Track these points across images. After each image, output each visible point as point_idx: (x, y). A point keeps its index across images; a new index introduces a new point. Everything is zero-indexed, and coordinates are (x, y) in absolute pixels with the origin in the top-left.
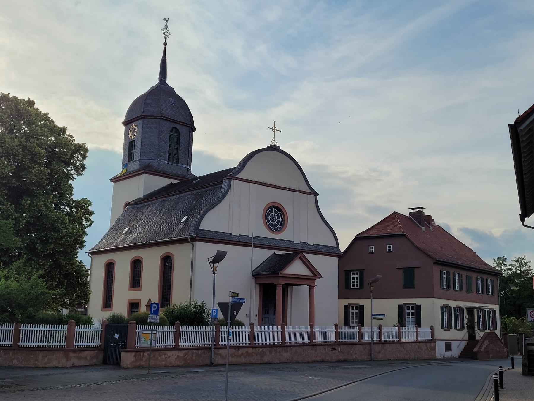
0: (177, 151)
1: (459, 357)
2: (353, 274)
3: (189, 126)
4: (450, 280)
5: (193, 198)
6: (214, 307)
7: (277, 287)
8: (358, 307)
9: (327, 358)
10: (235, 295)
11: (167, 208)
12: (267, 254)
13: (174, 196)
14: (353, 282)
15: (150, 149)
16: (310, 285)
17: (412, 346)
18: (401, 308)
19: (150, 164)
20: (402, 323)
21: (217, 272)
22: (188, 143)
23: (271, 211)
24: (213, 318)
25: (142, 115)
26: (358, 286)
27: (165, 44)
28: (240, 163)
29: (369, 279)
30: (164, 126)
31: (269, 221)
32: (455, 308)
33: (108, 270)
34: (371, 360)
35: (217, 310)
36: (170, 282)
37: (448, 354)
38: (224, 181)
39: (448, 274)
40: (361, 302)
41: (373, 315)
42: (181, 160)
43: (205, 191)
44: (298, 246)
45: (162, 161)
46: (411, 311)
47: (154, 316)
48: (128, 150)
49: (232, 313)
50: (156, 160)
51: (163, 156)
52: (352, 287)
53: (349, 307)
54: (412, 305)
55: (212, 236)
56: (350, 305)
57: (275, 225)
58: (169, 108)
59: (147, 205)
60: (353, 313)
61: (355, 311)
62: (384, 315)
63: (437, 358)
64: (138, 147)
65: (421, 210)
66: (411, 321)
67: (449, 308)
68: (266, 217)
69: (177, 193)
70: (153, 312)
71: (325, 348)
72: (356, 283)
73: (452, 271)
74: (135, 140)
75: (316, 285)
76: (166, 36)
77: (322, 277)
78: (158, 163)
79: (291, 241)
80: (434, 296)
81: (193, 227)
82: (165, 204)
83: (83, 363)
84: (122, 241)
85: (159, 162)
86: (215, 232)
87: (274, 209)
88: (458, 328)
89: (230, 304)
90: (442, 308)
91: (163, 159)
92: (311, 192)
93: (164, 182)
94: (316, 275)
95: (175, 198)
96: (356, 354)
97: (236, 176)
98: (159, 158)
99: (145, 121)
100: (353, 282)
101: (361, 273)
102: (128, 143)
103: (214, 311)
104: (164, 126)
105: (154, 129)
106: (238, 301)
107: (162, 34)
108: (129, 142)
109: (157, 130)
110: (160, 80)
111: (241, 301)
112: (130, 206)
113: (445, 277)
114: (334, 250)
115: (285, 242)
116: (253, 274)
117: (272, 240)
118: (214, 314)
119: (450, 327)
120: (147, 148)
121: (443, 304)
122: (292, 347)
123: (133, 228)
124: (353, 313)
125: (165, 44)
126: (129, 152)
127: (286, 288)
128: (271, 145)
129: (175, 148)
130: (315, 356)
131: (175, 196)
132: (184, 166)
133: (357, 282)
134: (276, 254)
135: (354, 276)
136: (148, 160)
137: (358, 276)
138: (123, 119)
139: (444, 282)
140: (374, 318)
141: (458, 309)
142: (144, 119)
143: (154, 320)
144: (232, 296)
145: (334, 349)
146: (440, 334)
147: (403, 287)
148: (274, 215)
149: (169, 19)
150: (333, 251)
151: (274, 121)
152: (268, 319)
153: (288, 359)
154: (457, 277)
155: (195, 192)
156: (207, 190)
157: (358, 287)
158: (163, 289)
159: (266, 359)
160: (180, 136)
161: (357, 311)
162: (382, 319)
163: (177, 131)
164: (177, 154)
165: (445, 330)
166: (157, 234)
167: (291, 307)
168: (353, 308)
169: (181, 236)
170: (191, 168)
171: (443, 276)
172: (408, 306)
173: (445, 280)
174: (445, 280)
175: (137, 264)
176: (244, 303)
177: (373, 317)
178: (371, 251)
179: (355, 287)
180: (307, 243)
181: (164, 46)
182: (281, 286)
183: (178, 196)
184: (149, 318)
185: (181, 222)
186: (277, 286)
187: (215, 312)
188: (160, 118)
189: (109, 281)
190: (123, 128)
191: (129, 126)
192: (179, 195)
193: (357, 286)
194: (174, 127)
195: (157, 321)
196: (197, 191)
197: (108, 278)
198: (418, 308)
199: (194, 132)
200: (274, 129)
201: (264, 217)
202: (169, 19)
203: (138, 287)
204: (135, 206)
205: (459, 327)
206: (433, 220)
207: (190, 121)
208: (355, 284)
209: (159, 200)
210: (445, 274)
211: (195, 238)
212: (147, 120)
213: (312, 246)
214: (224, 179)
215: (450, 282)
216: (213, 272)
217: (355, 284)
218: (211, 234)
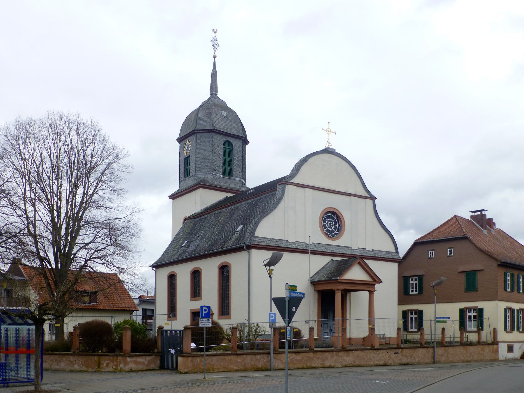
0: (231, 164)
1: (521, 358)
2: (412, 280)
3: (242, 139)
4: (514, 282)
5: (248, 207)
6: (271, 311)
7: (336, 293)
8: (417, 312)
9: (390, 362)
10: (292, 288)
11: (223, 219)
12: (325, 260)
13: (229, 207)
14: (413, 288)
15: (204, 163)
16: (370, 290)
17: (475, 348)
18: (462, 312)
19: (205, 179)
20: (463, 326)
21: (273, 274)
22: (241, 155)
23: (328, 217)
24: (271, 322)
25: (195, 129)
26: (417, 292)
27: (215, 57)
28: (294, 168)
29: (432, 282)
30: (217, 140)
31: (325, 227)
32: (518, 311)
33: (171, 282)
34: (434, 363)
35: (275, 314)
36: (229, 291)
37: (510, 356)
38: (278, 186)
39: (512, 276)
40: (420, 307)
41: (436, 318)
42: (235, 173)
43: (260, 200)
44: (356, 252)
45: (217, 175)
46: (472, 314)
47: (205, 319)
48: (183, 166)
49: (290, 309)
50: (211, 174)
51: (218, 170)
52: (411, 293)
53: (408, 312)
54: (474, 308)
55: (268, 244)
56: (409, 310)
57: (332, 232)
58: (221, 120)
59: (204, 218)
60: (412, 318)
61: (414, 316)
62: (449, 318)
63: (499, 359)
64: (193, 162)
65: (483, 212)
66: (472, 324)
67: (512, 310)
68: (323, 223)
69: (232, 203)
70: (203, 316)
71: (388, 351)
72: (415, 289)
73: (516, 273)
74: (189, 156)
75: (376, 291)
76: (215, 48)
77: (381, 282)
78: (213, 177)
79: (349, 247)
80: (498, 299)
81: (249, 235)
82: (220, 216)
83: (140, 367)
84: (182, 253)
85: (214, 176)
86: (271, 239)
87: (330, 215)
88: (508, 330)
89: (287, 299)
90: (505, 310)
91: (217, 173)
92: (368, 196)
93: (220, 196)
94: (375, 280)
95: (230, 209)
96: (419, 357)
97: (291, 181)
98: (213, 172)
99: (199, 136)
100: (413, 288)
101: (420, 278)
102: (184, 159)
103: (271, 315)
104: (217, 140)
105: (207, 143)
106: (296, 295)
107: (211, 46)
108: (185, 158)
109: (211, 144)
110: (212, 94)
111: (300, 295)
112: (188, 221)
113: (509, 280)
114: (393, 255)
115: (343, 248)
116: (311, 281)
117: (330, 246)
118: (271, 318)
119: (512, 329)
120: (201, 162)
121: (507, 307)
122: (354, 351)
123: (193, 241)
124: (412, 318)
125: (215, 57)
126: (185, 168)
127: (345, 294)
128: (326, 148)
129: (229, 161)
130: (377, 360)
131: (231, 207)
132: (239, 179)
133: (416, 288)
134: (334, 260)
135: (413, 282)
136: (203, 175)
137: (417, 282)
138: (177, 136)
139: (508, 285)
140: (438, 322)
141: (521, 311)
142: (197, 134)
143: (206, 324)
144: (289, 290)
145: (397, 353)
146: (502, 336)
147: (465, 291)
148: (331, 221)
149: (217, 30)
150: (392, 256)
151: (328, 122)
152: (327, 325)
153: (350, 363)
154: (521, 279)
155: (249, 201)
156: (261, 198)
157: (417, 293)
158: (222, 298)
159: (327, 364)
160: (233, 149)
161: (416, 316)
162: (446, 322)
163: (230, 144)
164: (231, 168)
165: (508, 332)
166: (213, 245)
167: (350, 313)
168: (412, 314)
169: (237, 245)
170: (245, 181)
171: (507, 278)
172: (470, 309)
173: (509, 283)
174: (509, 283)
175: (196, 275)
176: (304, 298)
177: (437, 320)
178: (431, 256)
179: (414, 293)
180: (365, 249)
181: (214, 59)
182: (340, 292)
183: (233, 207)
184: (200, 321)
185: (237, 231)
186: (336, 291)
187: (272, 317)
188: (213, 131)
189: (173, 292)
190: (178, 144)
191: (183, 142)
192: (234, 206)
193: (416, 291)
194: (227, 140)
195: (209, 325)
196: (252, 200)
197: (171, 290)
198: (480, 311)
199: (247, 146)
200: (329, 131)
201: (320, 224)
202: (217, 30)
203: (198, 297)
204: (193, 220)
205: (522, 329)
206: (494, 224)
207: (243, 133)
208: (414, 289)
209: (215, 212)
210: (509, 277)
211: (251, 245)
212: (200, 134)
213: (370, 252)
214: (278, 185)
215: (514, 284)
216: (269, 275)
217: (414, 289)
218: (267, 241)
